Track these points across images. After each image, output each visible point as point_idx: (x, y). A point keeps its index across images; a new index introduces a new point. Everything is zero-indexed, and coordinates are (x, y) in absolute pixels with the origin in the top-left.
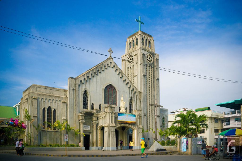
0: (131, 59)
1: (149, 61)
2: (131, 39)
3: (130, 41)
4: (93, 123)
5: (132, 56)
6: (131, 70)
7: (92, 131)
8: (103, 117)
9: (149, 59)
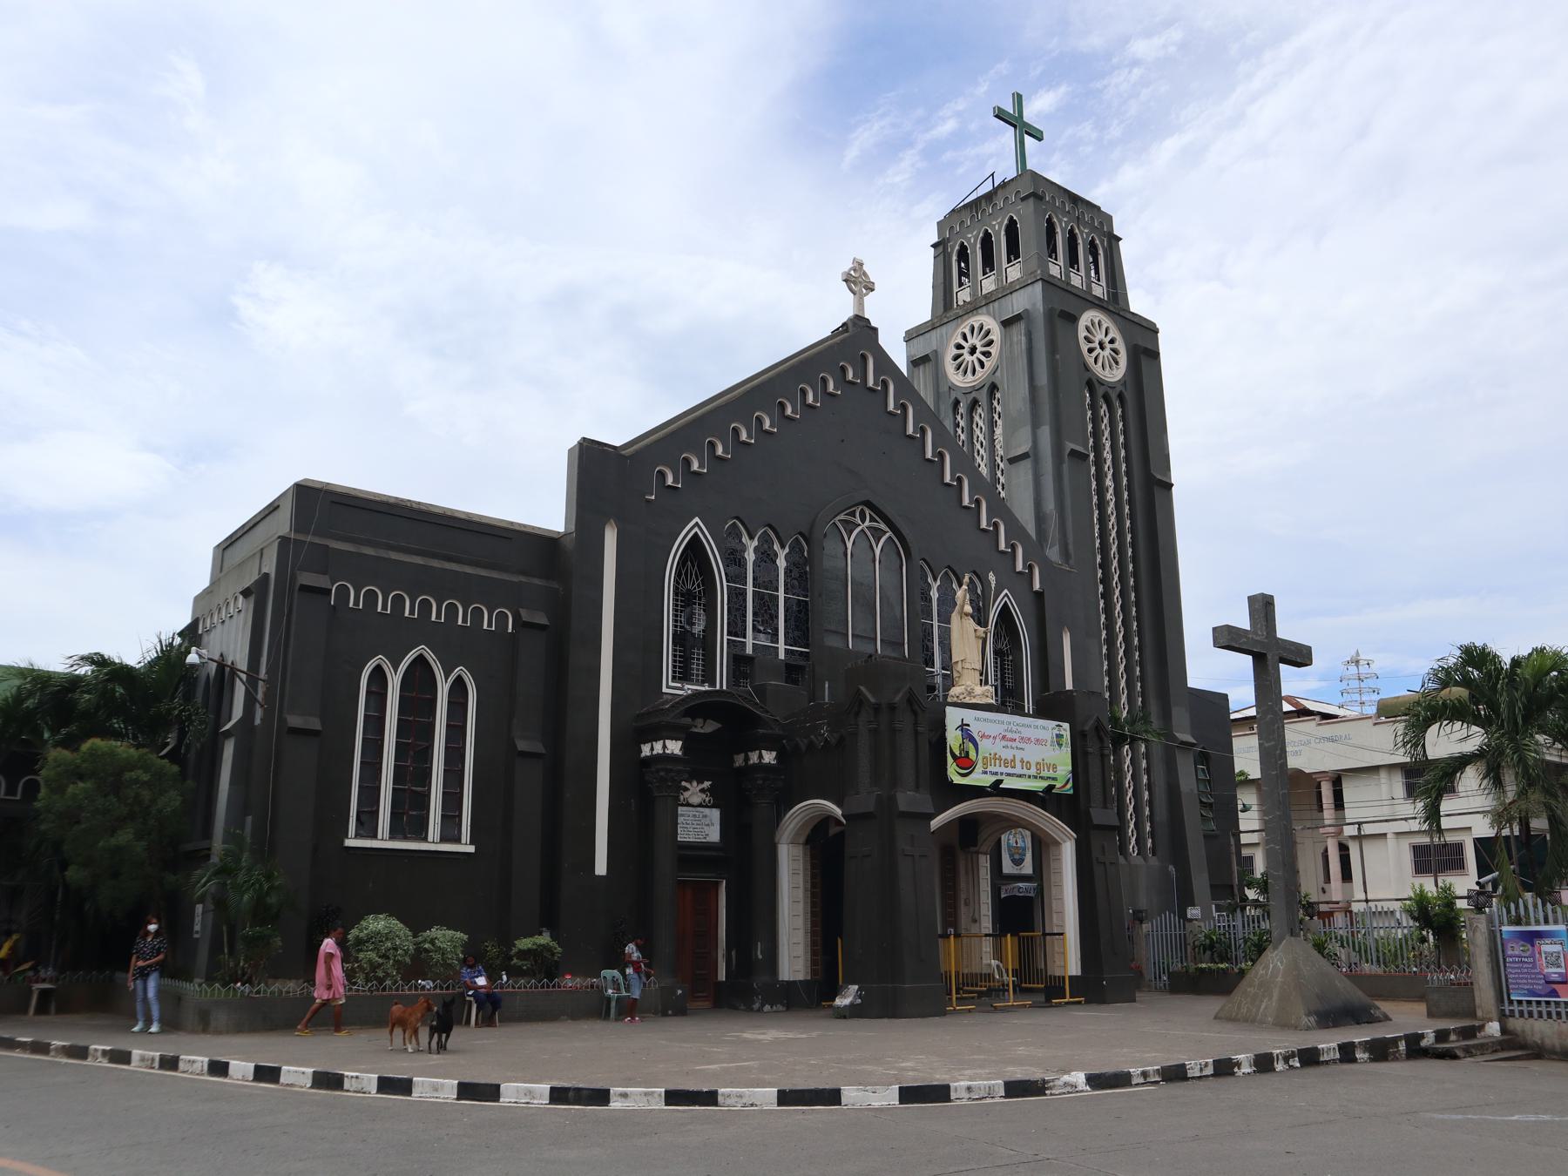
0: (980, 349)
1: (1100, 364)
5: (981, 328)
9: (1102, 348)
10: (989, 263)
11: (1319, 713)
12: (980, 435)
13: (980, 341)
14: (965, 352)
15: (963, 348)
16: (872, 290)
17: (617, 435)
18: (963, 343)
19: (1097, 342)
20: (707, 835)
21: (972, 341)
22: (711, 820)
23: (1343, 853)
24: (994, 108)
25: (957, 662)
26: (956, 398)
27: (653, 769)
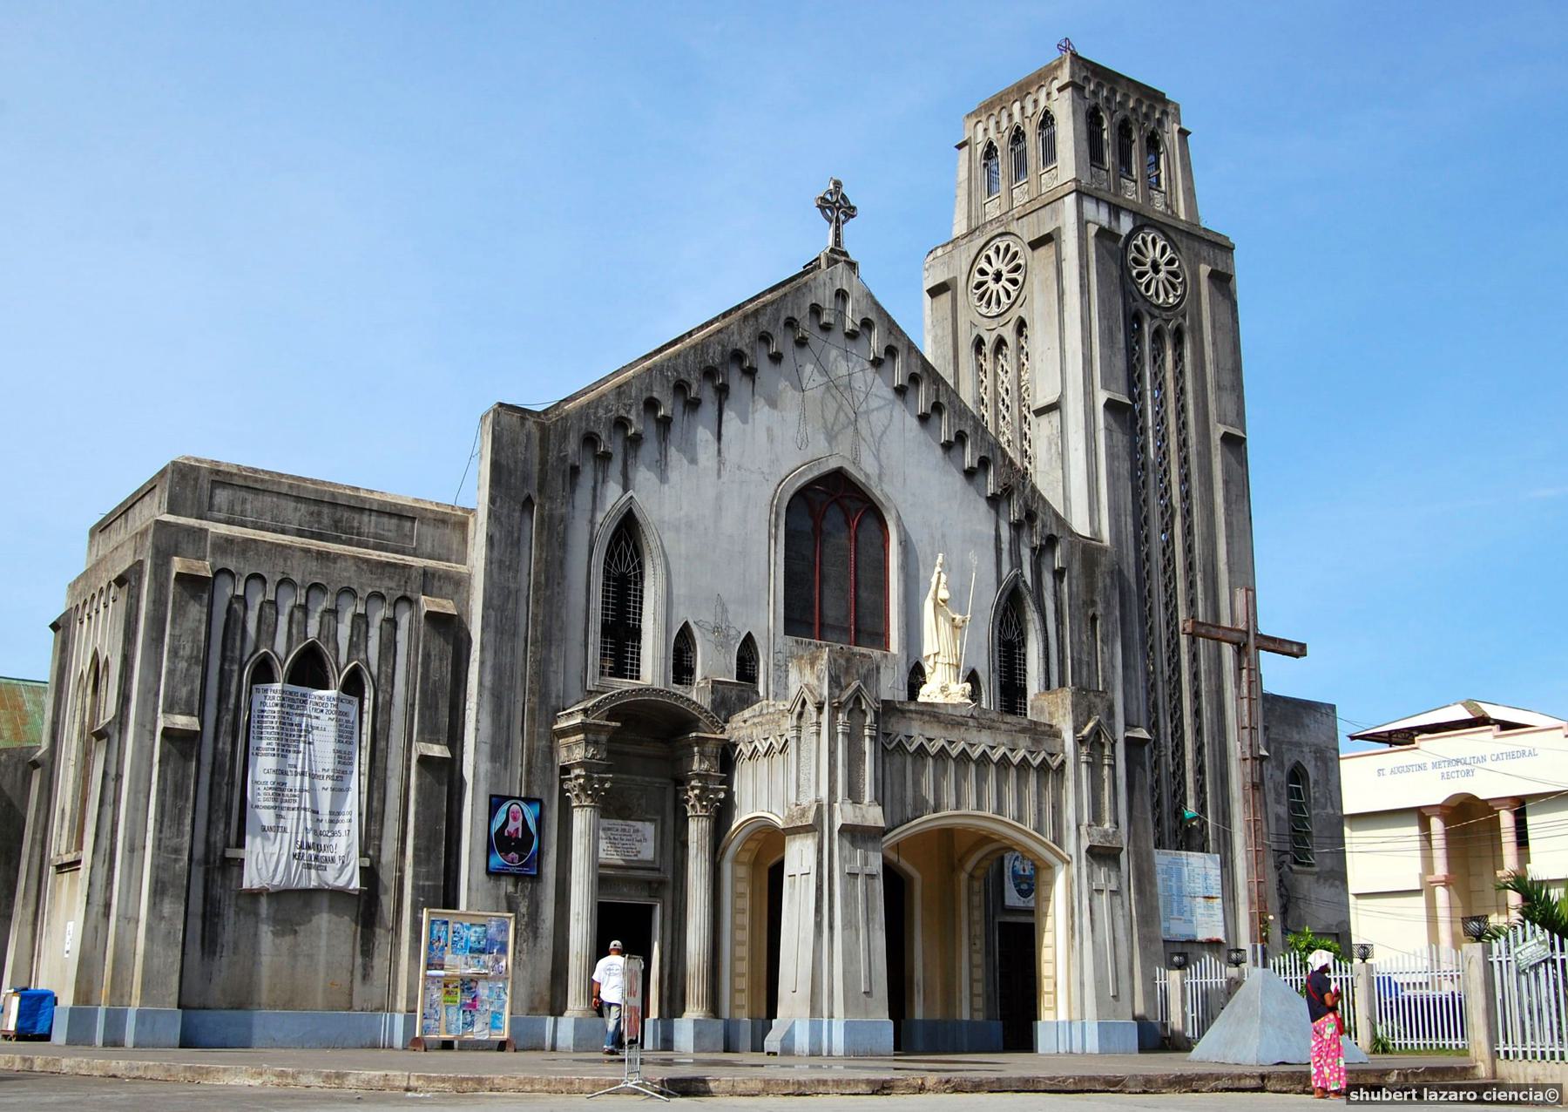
2: (997, 123)
3: (992, 134)
10: (1020, 167)
11: (1497, 722)
12: (1006, 381)
15: (987, 274)
16: (853, 216)
17: (538, 401)
19: (1149, 264)
20: (639, 852)
21: (998, 264)
22: (644, 835)
26: (978, 335)
27: (572, 776)
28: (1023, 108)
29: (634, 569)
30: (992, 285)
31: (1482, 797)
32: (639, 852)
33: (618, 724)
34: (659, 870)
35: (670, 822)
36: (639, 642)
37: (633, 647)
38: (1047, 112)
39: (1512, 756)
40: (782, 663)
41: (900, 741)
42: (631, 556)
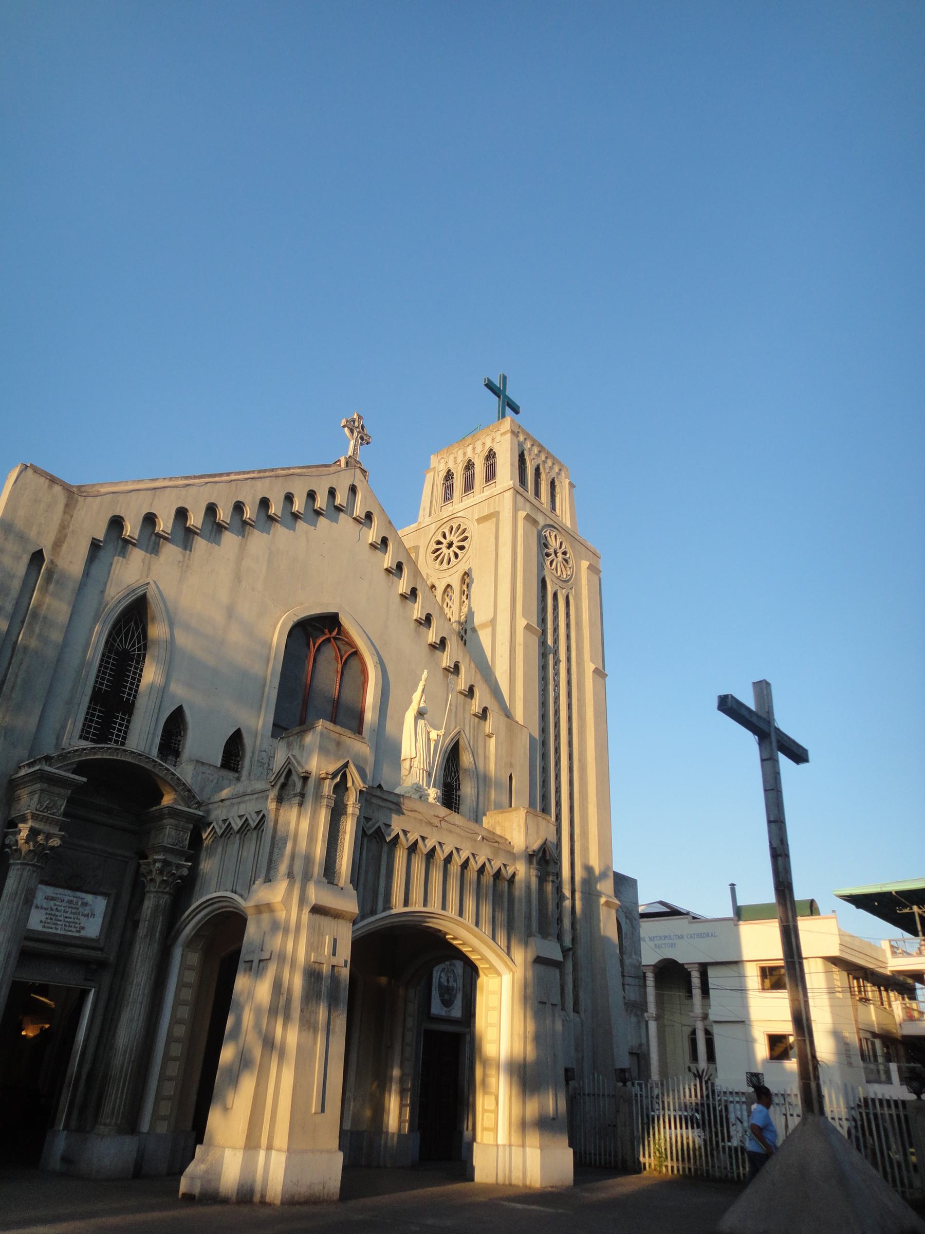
0: (456, 544)
2: (455, 458)
3: (451, 465)
4: (143, 869)
6: (447, 600)
7: (112, 958)
8: (253, 825)
9: (556, 553)
13: (458, 541)
14: (444, 547)
18: (442, 540)
20: (83, 928)
23: (708, 1037)
24: (485, 379)
25: (405, 760)
28: (474, 449)
29: (139, 649)
30: (444, 550)
31: (680, 962)
32: (83, 928)
33: (85, 779)
34: (101, 949)
35: (125, 898)
36: (130, 716)
37: (122, 719)
38: (491, 450)
39: (700, 936)
40: (265, 761)
41: (379, 827)
42: (138, 637)
